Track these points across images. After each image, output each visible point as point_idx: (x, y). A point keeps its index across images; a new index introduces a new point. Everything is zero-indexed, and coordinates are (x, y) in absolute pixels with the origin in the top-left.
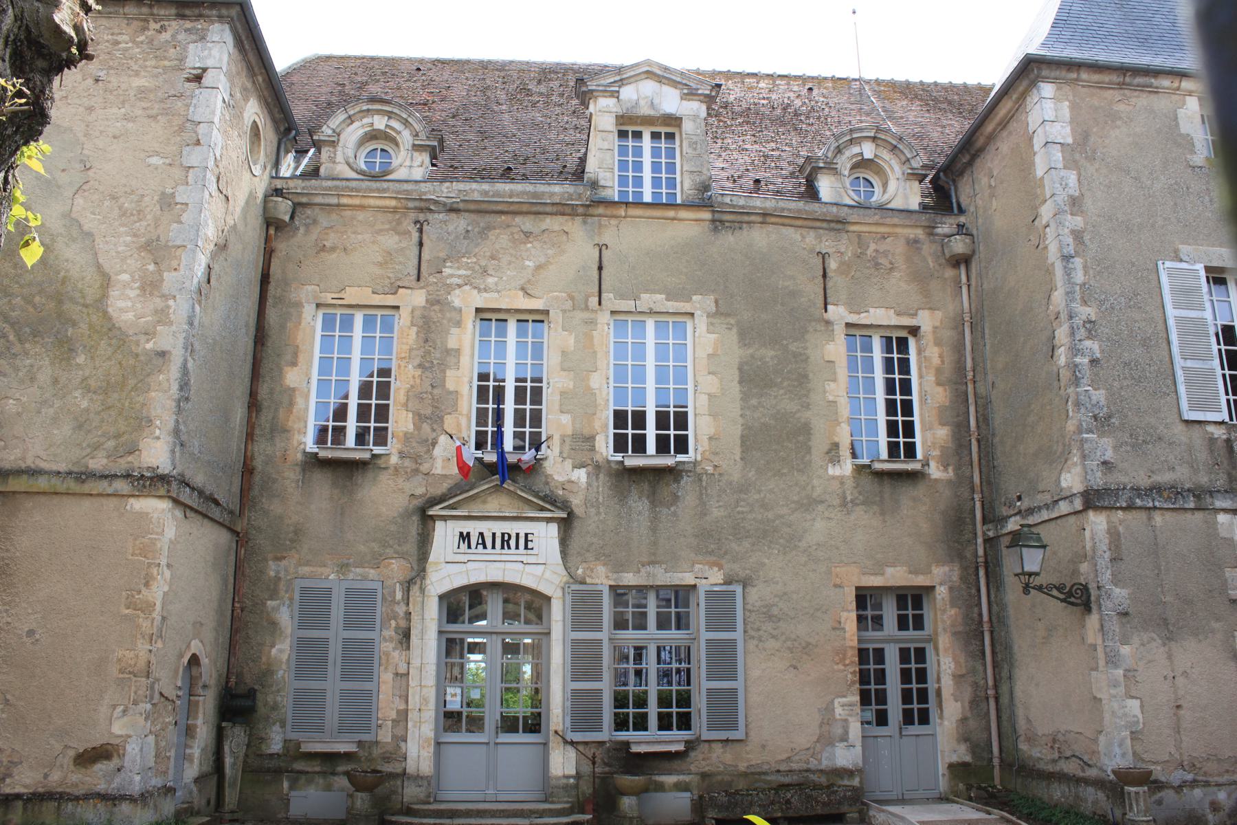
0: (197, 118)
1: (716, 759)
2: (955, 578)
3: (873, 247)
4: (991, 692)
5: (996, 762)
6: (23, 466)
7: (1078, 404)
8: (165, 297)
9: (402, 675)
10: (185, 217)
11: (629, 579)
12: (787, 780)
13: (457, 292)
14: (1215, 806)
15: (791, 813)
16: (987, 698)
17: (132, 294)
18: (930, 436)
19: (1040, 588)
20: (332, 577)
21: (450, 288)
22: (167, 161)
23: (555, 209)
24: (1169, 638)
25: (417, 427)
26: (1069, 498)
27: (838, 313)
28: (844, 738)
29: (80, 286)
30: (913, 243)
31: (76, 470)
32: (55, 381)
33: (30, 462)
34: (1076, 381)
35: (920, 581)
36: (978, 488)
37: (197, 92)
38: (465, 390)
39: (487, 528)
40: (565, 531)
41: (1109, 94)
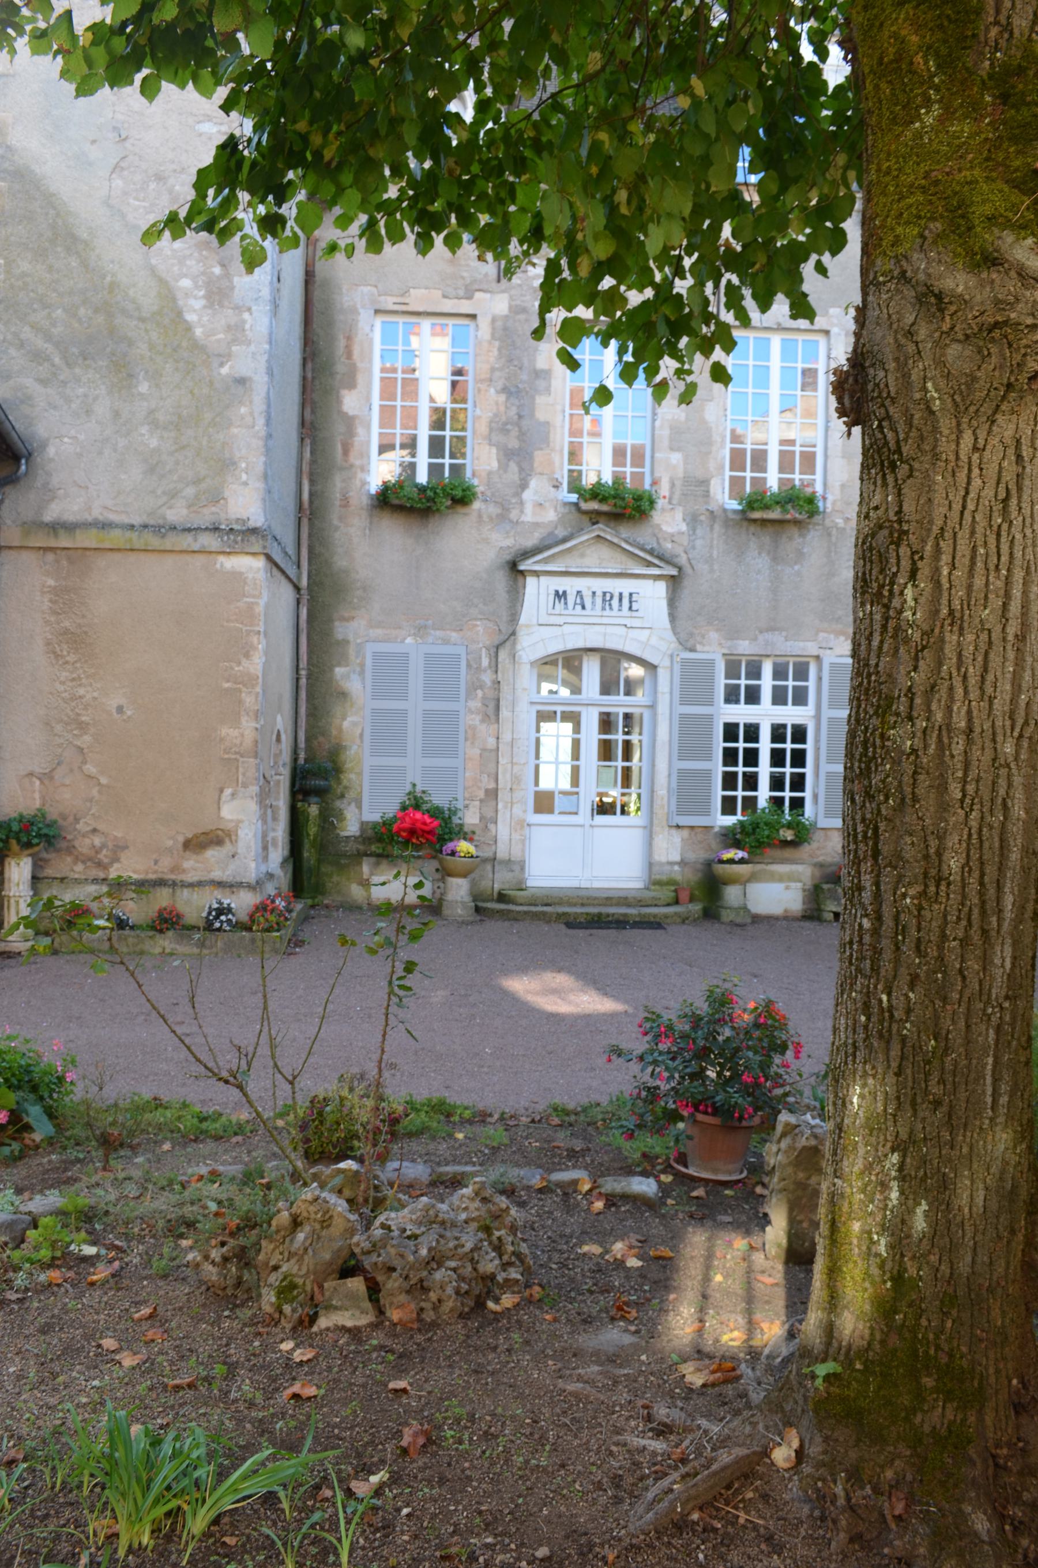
6: (90, 519)
8: (238, 309)
11: (745, 647)
29: (131, 292)
31: (152, 522)
32: (117, 414)
33: (97, 513)
38: (557, 421)
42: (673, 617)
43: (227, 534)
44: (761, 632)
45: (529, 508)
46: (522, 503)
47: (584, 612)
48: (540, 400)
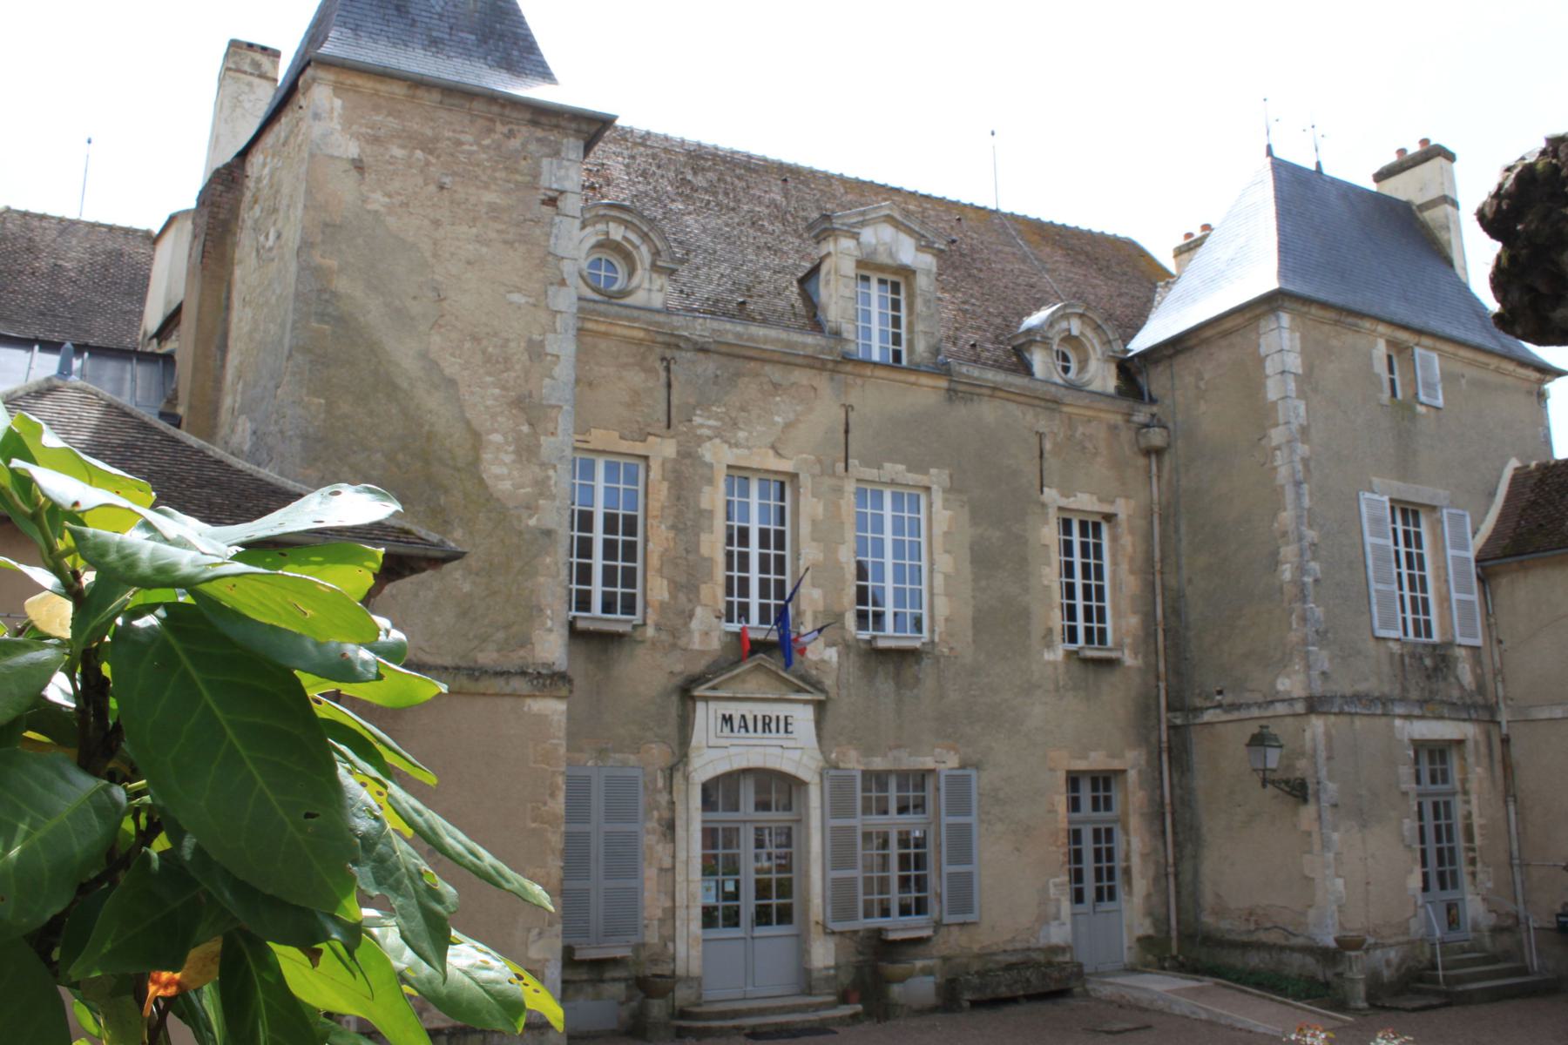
0: (560, 253)
1: (955, 942)
2: (1143, 762)
3: (1080, 430)
4: (1171, 870)
5: (1174, 934)
7: (1304, 619)
8: (542, 465)
9: (666, 870)
10: (557, 371)
11: (878, 763)
12: (1013, 959)
13: (708, 444)
14: (1388, 963)
15: (1031, 991)
16: (1167, 875)
17: (508, 458)
18: (1121, 625)
19: (1273, 782)
20: (590, 763)
21: (700, 440)
22: (531, 300)
23: (805, 361)
24: (1364, 826)
25: (673, 596)
26: (1291, 701)
27: (1051, 495)
28: (1057, 917)
30: (1113, 428)
31: (463, 664)
34: (1304, 599)
35: (1116, 764)
36: (1162, 676)
37: (557, 219)
39: (749, 710)
41: (1326, 328)
45: (697, 637)
46: (689, 631)
48: (704, 537)
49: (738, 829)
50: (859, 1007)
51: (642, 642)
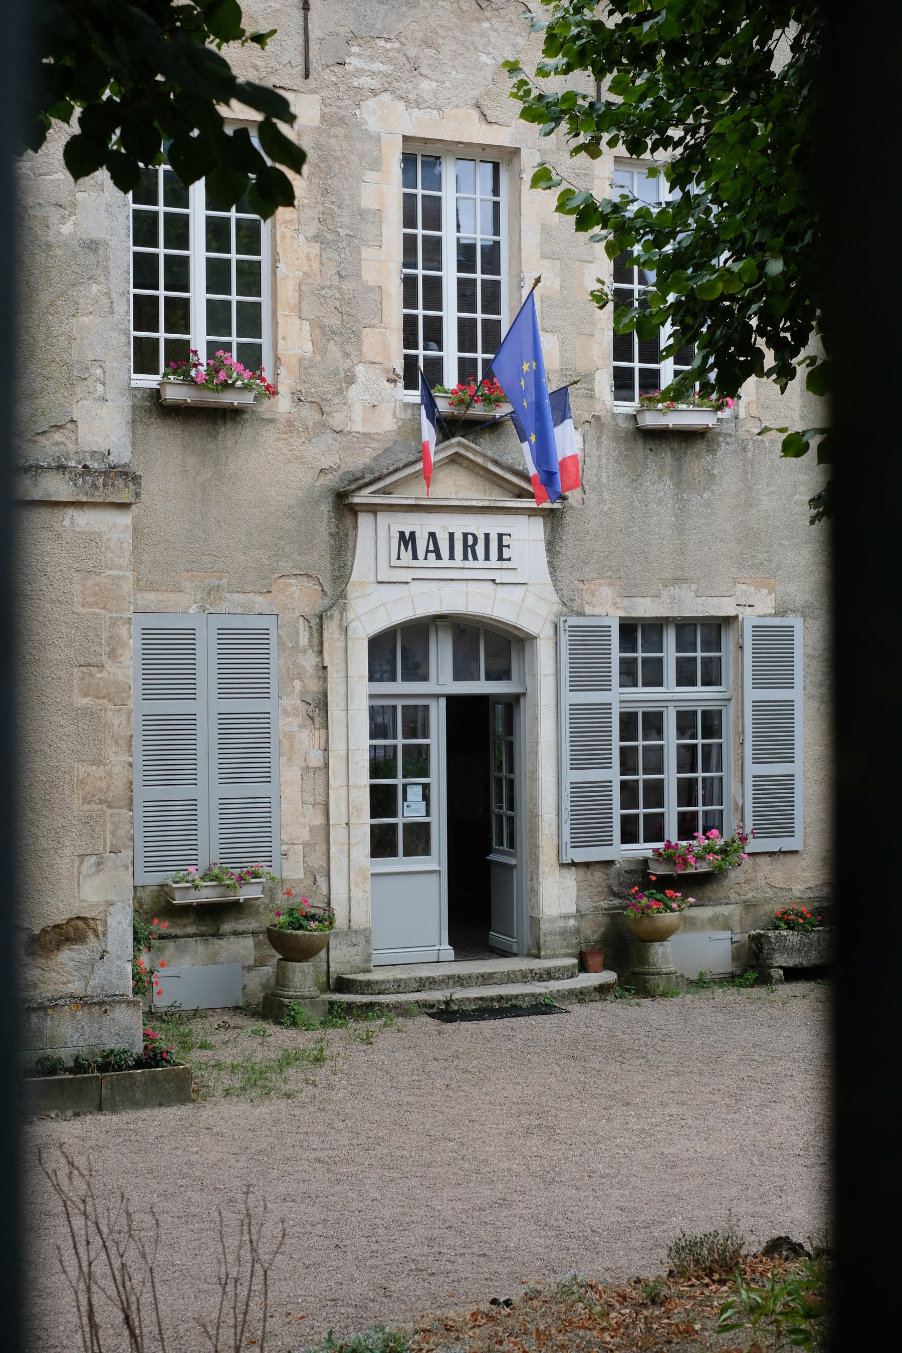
13: (371, 103)
21: (359, 95)
25: (320, 349)
40: (553, 530)
42: (553, 567)
43: (82, 475)
44: (666, 586)
45: (358, 412)
47: (439, 564)
48: (367, 253)
49: (426, 708)
50: (609, 976)
51: (272, 421)
